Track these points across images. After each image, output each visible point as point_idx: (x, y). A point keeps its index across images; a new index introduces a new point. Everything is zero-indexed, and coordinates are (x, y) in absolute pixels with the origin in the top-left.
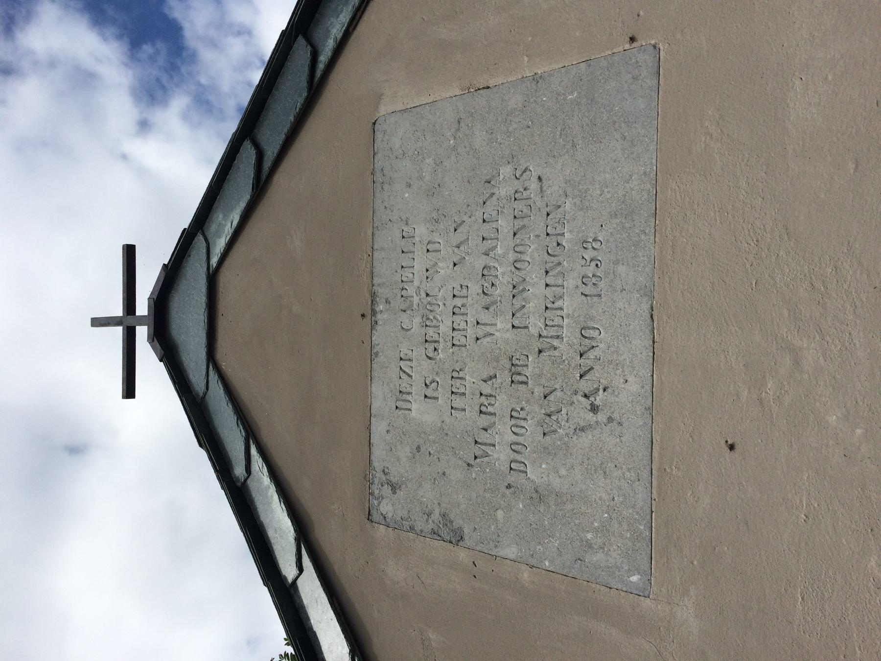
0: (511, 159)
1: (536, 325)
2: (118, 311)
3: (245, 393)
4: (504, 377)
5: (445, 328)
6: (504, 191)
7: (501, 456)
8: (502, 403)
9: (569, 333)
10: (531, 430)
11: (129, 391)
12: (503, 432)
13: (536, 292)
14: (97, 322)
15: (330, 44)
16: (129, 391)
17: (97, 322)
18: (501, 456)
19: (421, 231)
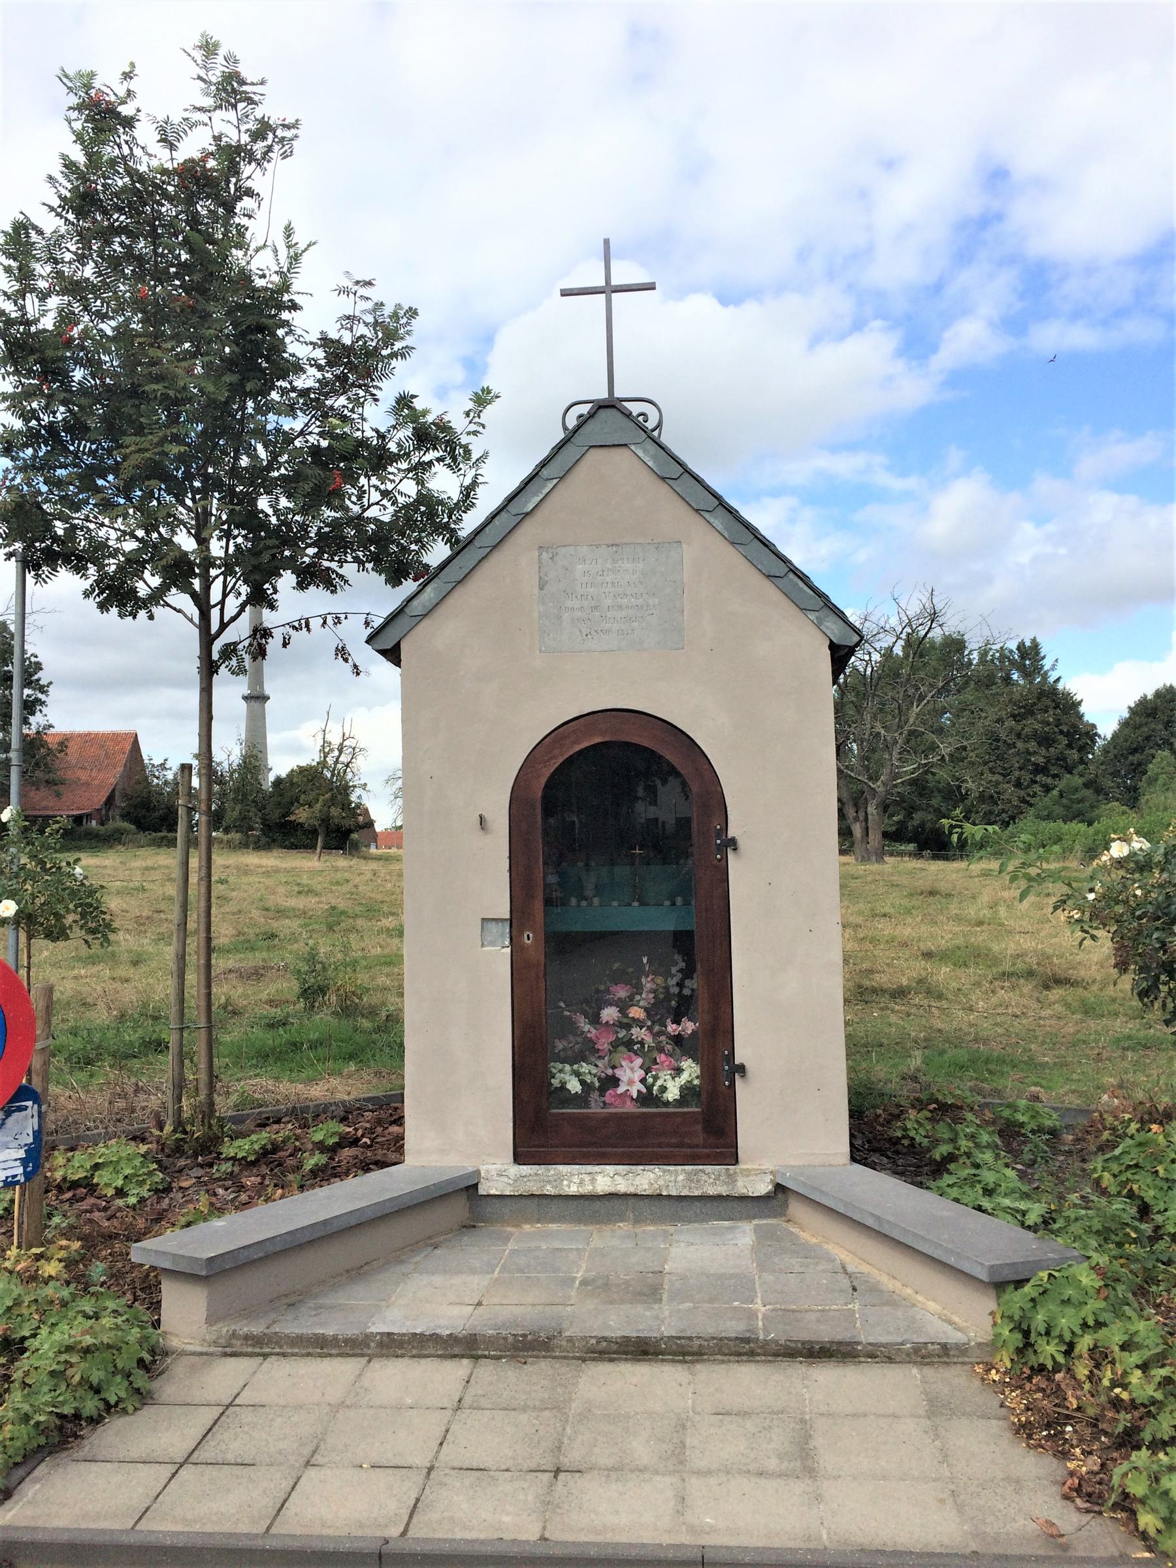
0: (660, 604)
1: (609, 614)
2: (615, 281)
3: (545, 505)
4: (593, 603)
5: (608, 579)
6: (651, 602)
7: (569, 604)
8: (586, 603)
9: (608, 626)
10: (578, 614)
11: (565, 293)
12: (576, 604)
13: (621, 614)
14: (51, 683)
15: (712, 520)
16: (565, 293)
17: (51, 683)
18: (569, 604)
19: (640, 566)
